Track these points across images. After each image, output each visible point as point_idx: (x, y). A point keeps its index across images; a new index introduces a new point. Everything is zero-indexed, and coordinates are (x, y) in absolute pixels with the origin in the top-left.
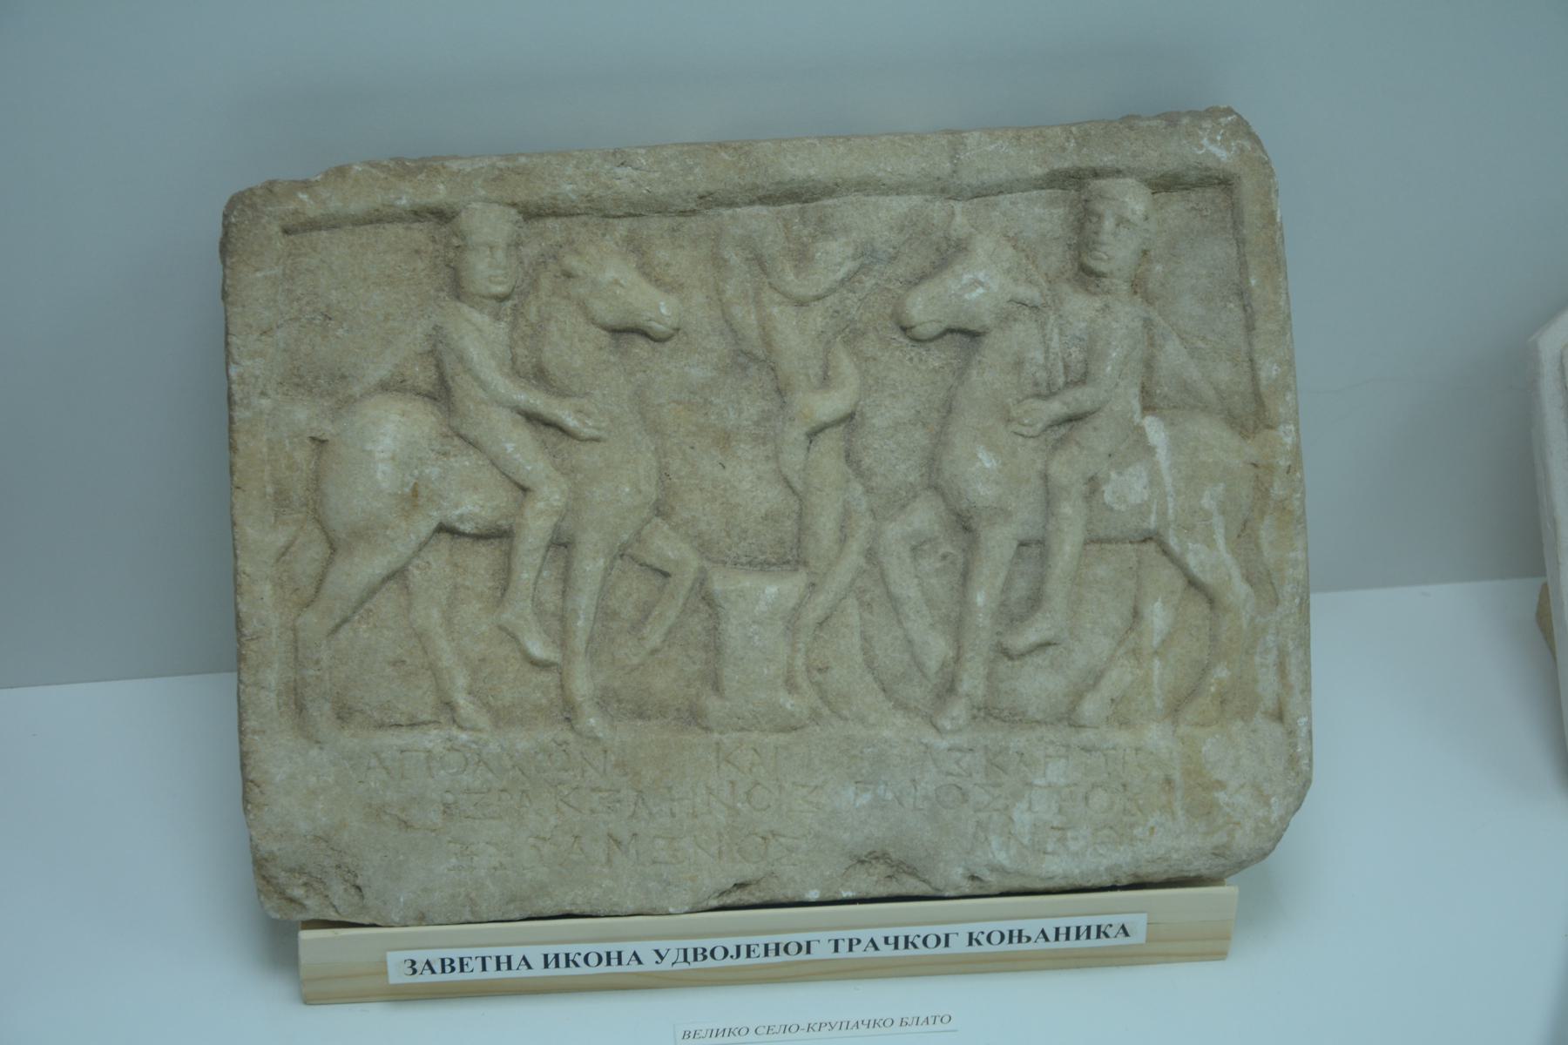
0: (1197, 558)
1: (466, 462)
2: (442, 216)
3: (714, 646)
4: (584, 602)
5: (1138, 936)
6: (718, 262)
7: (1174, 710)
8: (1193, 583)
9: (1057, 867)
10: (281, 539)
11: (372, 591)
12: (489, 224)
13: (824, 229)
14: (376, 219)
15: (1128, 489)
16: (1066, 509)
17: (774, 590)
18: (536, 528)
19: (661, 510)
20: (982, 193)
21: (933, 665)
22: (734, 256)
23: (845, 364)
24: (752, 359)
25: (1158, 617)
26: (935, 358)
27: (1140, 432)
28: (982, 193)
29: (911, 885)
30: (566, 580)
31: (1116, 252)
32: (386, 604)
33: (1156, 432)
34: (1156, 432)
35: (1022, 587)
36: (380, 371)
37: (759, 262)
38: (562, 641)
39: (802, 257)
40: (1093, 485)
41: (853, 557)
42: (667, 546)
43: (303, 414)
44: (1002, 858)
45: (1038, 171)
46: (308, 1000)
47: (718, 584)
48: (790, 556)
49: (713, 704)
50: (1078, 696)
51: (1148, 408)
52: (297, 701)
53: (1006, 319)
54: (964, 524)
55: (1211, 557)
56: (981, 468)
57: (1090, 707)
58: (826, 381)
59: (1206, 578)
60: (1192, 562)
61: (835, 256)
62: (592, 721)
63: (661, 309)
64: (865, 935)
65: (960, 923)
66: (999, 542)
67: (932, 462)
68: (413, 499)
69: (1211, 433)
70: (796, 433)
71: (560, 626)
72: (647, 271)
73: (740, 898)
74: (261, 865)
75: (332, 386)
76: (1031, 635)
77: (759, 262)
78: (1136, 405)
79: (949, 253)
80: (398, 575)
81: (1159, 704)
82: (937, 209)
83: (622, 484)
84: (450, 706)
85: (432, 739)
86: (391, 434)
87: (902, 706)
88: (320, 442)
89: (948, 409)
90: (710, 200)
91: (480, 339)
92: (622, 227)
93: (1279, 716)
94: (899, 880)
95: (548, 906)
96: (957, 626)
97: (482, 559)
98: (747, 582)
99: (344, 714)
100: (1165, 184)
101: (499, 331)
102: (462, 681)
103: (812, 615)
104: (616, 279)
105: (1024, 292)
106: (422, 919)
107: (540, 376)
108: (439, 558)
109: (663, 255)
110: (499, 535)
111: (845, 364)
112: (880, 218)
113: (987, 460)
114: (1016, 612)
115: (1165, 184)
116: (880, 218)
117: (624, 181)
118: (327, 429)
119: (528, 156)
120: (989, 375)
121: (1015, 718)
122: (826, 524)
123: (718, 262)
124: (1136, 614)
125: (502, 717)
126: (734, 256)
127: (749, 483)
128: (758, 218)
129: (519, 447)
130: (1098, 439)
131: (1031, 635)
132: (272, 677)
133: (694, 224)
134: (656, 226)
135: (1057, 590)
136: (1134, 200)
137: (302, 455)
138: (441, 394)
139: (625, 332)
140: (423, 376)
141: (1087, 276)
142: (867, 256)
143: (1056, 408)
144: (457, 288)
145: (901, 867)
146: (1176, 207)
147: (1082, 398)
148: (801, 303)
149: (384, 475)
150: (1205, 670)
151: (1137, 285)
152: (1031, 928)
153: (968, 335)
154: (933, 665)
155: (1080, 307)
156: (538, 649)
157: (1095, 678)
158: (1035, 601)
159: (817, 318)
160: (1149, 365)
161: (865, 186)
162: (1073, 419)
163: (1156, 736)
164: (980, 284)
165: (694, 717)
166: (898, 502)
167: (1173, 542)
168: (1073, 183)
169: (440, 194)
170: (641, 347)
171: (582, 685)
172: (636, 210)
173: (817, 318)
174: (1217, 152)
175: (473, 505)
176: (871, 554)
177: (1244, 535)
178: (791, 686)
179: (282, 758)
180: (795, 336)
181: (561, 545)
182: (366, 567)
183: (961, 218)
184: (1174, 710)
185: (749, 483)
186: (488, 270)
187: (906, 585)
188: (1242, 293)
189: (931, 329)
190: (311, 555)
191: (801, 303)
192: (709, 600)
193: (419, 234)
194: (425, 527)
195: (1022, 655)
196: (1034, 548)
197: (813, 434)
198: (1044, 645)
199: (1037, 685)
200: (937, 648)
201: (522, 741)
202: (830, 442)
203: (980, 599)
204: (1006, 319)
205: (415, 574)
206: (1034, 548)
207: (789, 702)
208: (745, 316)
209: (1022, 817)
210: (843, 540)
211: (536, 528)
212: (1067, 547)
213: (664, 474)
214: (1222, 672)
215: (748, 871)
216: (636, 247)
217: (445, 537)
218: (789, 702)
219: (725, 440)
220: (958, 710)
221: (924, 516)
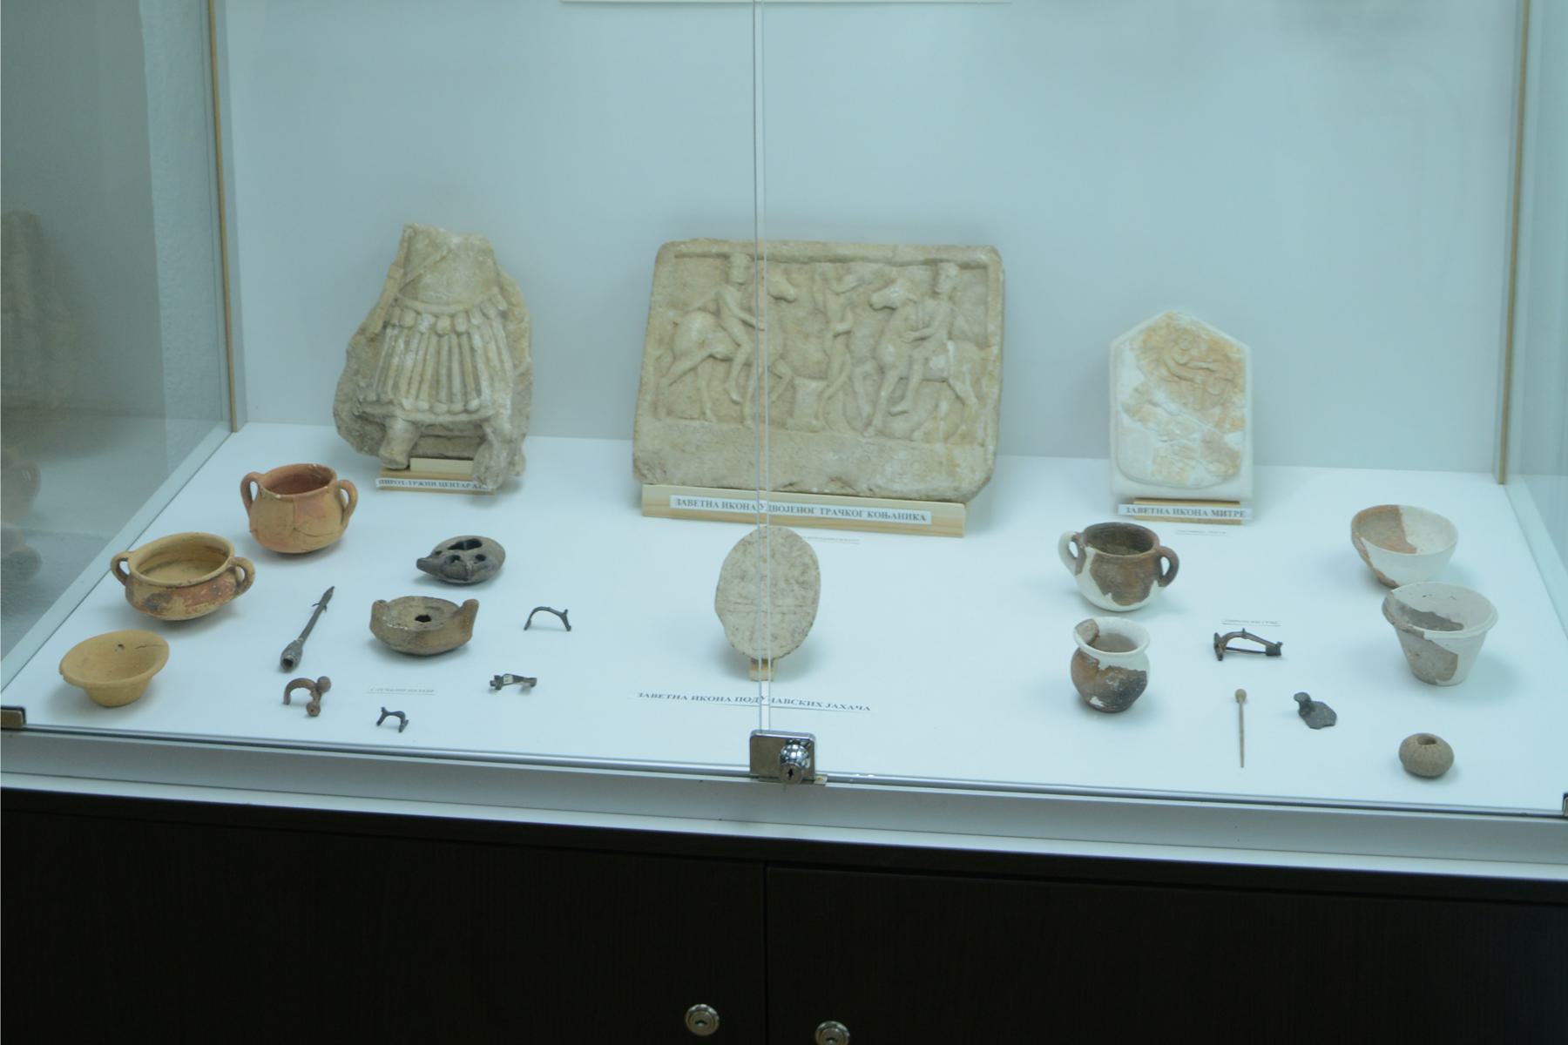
0: (959, 387)
1: (721, 334)
2: (725, 257)
3: (793, 402)
4: (752, 383)
5: (928, 522)
6: (812, 279)
7: (947, 438)
8: (958, 397)
9: (898, 487)
10: (658, 353)
11: (685, 373)
12: (740, 260)
13: (849, 272)
14: (704, 255)
15: (938, 363)
16: (916, 367)
17: (814, 385)
18: (740, 358)
19: (782, 357)
20: (903, 265)
21: (865, 414)
22: (817, 278)
23: (849, 315)
24: (820, 311)
25: (944, 407)
26: (880, 316)
27: (944, 345)
28: (903, 265)
29: (850, 491)
30: (748, 377)
31: (945, 286)
32: (689, 378)
33: (951, 346)
34: (951, 346)
35: (899, 392)
36: (698, 304)
37: (826, 280)
38: (743, 396)
39: (840, 280)
40: (927, 359)
41: (843, 378)
42: (782, 368)
43: (671, 314)
44: (880, 483)
45: (921, 258)
46: (645, 514)
47: (798, 381)
48: (822, 376)
49: (790, 421)
50: (913, 431)
51: (950, 337)
52: (655, 407)
53: (904, 304)
54: (882, 370)
55: (964, 388)
56: (889, 351)
57: (917, 435)
58: (842, 320)
59: (962, 395)
60: (957, 389)
61: (850, 281)
62: (749, 422)
63: (791, 292)
64: (832, 508)
65: (865, 509)
66: (892, 377)
67: (874, 350)
68: (702, 344)
69: (970, 349)
70: (830, 335)
71: (743, 390)
72: (790, 281)
73: (790, 487)
74: (635, 461)
75: (683, 307)
76: (899, 408)
77: (826, 280)
78: (945, 337)
79: (889, 282)
80: (693, 369)
81: (1173, 407)
82: (887, 269)
83: (768, 346)
84: (704, 413)
85: (696, 424)
86: (698, 323)
87: (854, 429)
88: (676, 324)
89: (882, 333)
90: (812, 260)
91: (732, 296)
92: (783, 266)
93: (982, 445)
94: (845, 487)
95: (725, 483)
96: (874, 404)
97: (722, 367)
98: (807, 381)
99: (670, 413)
100: (965, 266)
101: (738, 295)
102: (709, 405)
103: (827, 394)
104: (778, 282)
105: (912, 296)
106: (684, 484)
107: (749, 310)
108: (709, 364)
109: (795, 275)
110: (727, 360)
111: (849, 315)
112: (867, 270)
113: (891, 349)
114: (893, 401)
115: (965, 266)
116: (867, 270)
117: (785, 251)
118: (678, 320)
119: (272, 499)
120: (897, 322)
121: (891, 436)
122: (836, 366)
123: (812, 279)
124: (937, 406)
125: (720, 419)
126: (817, 278)
127: (813, 351)
128: (828, 266)
129: (738, 331)
130: (929, 345)
131: (899, 408)
132: (649, 398)
133: (806, 267)
134: (794, 266)
135: (910, 394)
136: (952, 270)
137: (669, 327)
138: (717, 313)
139: (779, 299)
140: (712, 307)
141: (935, 294)
142: (861, 282)
143: (917, 334)
144: (727, 281)
145: (846, 484)
146: (968, 275)
147: (926, 332)
148: (838, 294)
149: (694, 335)
150: (958, 426)
151: (951, 298)
152: (890, 512)
153: (891, 309)
154: (865, 414)
155: (930, 304)
156: (735, 397)
157: (920, 425)
158: (902, 398)
159: (842, 299)
160: (952, 324)
161: (864, 259)
162: (923, 339)
163: (939, 447)
164: (896, 293)
165: (783, 425)
166: (861, 361)
167: (952, 381)
168: (933, 263)
169: (725, 249)
170: (784, 304)
171: (747, 410)
172: (790, 260)
173: (842, 299)
174: (983, 257)
175: (721, 349)
176: (850, 378)
177: (976, 383)
178: (817, 418)
179: (648, 425)
180: (834, 304)
181: (748, 365)
182: (684, 365)
183: (894, 272)
184: (947, 438)
185: (813, 351)
186: (737, 275)
187: (860, 387)
188: (986, 303)
189: (877, 306)
190: (668, 359)
191: (838, 294)
192: (793, 387)
193: (718, 262)
194: (705, 353)
195: (974, 494)
196: (903, 380)
197: (836, 336)
198: (903, 412)
199: (899, 425)
200: (867, 409)
201: (725, 427)
202: (841, 339)
203: (883, 393)
204: (904, 304)
205: (700, 370)
206: (903, 380)
207: (814, 422)
208: (819, 297)
209: (888, 469)
210: (841, 372)
211: (740, 358)
212: (915, 379)
213: (785, 345)
214: (964, 427)
215: (794, 479)
216: (787, 273)
217: (711, 361)
218: (814, 422)
219: (807, 336)
220: (871, 430)
221: (869, 367)
